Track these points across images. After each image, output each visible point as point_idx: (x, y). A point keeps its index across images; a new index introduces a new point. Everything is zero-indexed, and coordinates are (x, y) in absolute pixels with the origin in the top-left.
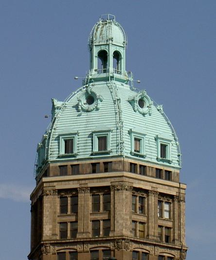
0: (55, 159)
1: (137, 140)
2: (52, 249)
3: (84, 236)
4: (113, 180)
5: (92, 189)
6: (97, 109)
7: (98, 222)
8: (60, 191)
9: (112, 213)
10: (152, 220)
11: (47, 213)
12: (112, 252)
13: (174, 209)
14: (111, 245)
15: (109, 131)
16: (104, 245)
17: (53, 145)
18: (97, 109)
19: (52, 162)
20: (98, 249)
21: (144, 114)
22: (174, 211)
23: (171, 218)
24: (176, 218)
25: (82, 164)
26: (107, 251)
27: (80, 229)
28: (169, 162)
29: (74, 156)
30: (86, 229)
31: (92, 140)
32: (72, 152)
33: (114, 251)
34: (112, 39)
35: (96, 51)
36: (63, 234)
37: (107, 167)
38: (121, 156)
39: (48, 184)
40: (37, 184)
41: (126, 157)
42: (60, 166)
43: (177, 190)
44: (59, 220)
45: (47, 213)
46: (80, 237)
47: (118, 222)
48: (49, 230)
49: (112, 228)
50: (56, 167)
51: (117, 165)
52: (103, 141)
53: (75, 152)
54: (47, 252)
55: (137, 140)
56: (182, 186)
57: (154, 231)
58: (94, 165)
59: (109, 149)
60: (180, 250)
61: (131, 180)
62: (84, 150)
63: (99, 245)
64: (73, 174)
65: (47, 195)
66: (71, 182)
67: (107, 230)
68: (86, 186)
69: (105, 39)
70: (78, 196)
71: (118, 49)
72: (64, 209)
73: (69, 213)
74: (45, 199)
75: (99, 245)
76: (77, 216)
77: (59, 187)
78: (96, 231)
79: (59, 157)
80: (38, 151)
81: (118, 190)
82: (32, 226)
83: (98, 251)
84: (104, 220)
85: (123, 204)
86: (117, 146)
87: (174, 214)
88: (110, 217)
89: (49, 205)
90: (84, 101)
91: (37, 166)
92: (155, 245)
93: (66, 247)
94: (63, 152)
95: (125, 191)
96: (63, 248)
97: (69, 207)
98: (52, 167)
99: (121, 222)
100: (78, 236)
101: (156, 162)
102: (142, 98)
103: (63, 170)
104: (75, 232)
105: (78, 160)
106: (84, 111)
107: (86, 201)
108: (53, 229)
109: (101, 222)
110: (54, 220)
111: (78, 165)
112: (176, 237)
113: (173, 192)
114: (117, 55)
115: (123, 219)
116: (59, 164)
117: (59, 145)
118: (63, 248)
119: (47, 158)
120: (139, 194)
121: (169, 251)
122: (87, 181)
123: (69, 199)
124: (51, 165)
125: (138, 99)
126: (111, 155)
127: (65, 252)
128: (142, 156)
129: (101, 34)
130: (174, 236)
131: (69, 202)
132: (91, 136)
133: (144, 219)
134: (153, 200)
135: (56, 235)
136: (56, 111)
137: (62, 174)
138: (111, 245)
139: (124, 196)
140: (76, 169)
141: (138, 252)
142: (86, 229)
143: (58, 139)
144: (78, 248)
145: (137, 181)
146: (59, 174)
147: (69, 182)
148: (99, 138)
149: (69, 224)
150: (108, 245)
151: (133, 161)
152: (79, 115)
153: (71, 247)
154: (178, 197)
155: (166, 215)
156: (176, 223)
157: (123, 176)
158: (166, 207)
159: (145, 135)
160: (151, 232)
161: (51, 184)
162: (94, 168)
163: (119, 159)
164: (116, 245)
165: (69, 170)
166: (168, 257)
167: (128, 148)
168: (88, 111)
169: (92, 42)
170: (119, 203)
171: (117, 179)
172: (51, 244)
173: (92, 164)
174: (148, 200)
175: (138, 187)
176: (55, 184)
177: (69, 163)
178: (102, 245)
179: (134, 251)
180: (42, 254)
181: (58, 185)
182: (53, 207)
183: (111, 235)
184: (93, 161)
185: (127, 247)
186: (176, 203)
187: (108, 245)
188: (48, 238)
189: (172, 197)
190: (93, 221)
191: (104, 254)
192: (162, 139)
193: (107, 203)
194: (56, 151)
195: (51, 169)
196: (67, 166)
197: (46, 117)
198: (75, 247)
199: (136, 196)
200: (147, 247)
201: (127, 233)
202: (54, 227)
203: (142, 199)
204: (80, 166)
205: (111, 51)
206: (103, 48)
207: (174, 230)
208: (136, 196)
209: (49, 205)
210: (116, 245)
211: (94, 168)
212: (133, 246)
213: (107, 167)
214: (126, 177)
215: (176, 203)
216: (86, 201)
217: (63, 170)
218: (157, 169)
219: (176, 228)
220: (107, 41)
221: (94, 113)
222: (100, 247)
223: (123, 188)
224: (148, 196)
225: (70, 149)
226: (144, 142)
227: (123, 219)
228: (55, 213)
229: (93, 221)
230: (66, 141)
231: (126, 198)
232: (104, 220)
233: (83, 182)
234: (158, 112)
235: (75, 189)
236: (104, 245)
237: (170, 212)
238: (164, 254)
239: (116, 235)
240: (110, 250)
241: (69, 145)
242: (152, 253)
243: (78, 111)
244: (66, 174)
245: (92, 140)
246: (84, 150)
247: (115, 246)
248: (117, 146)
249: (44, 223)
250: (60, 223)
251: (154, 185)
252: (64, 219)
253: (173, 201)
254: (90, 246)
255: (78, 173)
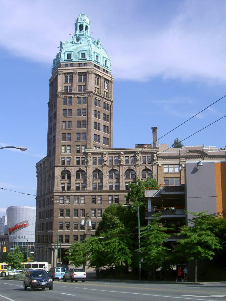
0: (63, 61)
1: (97, 56)
2: (61, 96)
3: (75, 91)
4: (88, 69)
5: (79, 73)
6: (81, 43)
7: (81, 87)
8: (65, 73)
9: (87, 82)
10: (102, 88)
11: (60, 82)
12: (87, 98)
13: (109, 85)
14: (86, 95)
15: (86, 51)
16: (84, 95)
17: (62, 56)
18: (81, 43)
19: (62, 62)
20: (81, 97)
21: (98, 48)
22: (109, 87)
23: (108, 89)
24: (110, 89)
25: (75, 64)
26: (85, 98)
27: (73, 88)
28: (108, 67)
29: (71, 60)
30: (76, 89)
31: (79, 54)
32: (70, 58)
33: (88, 97)
34: (85, 20)
35: (78, 24)
36: (66, 90)
37: (85, 64)
38: (91, 61)
39: (60, 71)
40: (52, 75)
41: (93, 61)
42: (65, 64)
43: (110, 78)
44: (64, 85)
45: (60, 82)
46: (73, 91)
47: (89, 86)
48: (60, 88)
49: (87, 88)
50: (63, 64)
51: (89, 64)
52: (84, 55)
53: (72, 58)
54: (59, 97)
55: (97, 56)
56: (112, 77)
57: (102, 92)
58: (79, 64)
59: (86, 58)
60: (111, 101)
61: (95, 70)
62: (75, 58)
63: (81, 95)
64: (70, 67)
65: (60, 75)
66: (70, 70)
67: (85, 90)
68: (76, 71)
69: (82, 20)
70: (72, 76)
71: (87, 25)
72: (66, 81)
73: (68, 82)
74: (59, 76)
75: (81, 95)
76: (72, 83)
77: (65, 72)
78: (80, 90)
79: (65, 61)
80: (75, 24)
81: (90, 73)
82: (50, 91)
83: (81, 97)
84: (83, 86)
85: (92, 79)
86: (90, 57)
87: (109, 87)
88: (86, 84)
89: (60, 79)
90: (75, 39)
91: (52, 68)
92: (103, 98)
93: (67, 96)
94: (66, 59)
95: (93, 74)
96: (66, 96)
97: (69, 80)
98: (62, 64)
99: (91, 86)
100: (72, 91)
101: (103, 66)
102: (98, 42)
103: (66, 65)
104: (71, 90)
105: (73, 62)
106: (75, 44)
107: (76, 77)
108: (62, 88)
109: (82, 86)
110: (62, 85)
111: (73, 64)
112: (110, 97)
113: (109, 79)
114: (87, 27)
115: (92, 85)
116: (65, 63)
117: (65, 56)
118: (66, 96)
119: (60, 61)
120: (97, 77)
121: (107, 101)
122: (77, 70)
123: (69, 77)
124: (61, 63)
125: (97, 41)
126: (87, 60)
127: (67, 98)
128: (99, 63)
129: (81, 18)
130: (109, 96)
131: (69, 78)
132: (79, 53)
133: (99, 87)
134: (102, 80)
135: (63, 91)
136: (63, 45)
137: (66, 67)
138: (86, 95)
139: (92, 76)
140: (72, 65)
141: (97, 99)
142: (76, 89)
143: (65, 53)
144: (73, 96)
145: (97, 71)
146: (65, 67)
147: (69, 70)
148: (82, 54)
149: (68, 87)
150: (85, 95)
151: (96, 64)
152: (73, 45)
153: (69, 96)
154: (111, 81)
155: (106, 88)
156: (110, 91)
157: (92, 68)
158: (106, 85)
159: (100, 55)
160: (101, 93)
161: (62, 71)
162: (80, 65)
163: (90, 62)
164: (89, 95)
165: (69, 65)
166: (107, 104)
167: (94, 58)
168: (77, 44)
169: (77, 21)
170: (90, 78)
171: (90, 69)
172: (61, 94)
173: (79, 63)
174: (100, 80)
175: (97, 73)
176: (63, 70)
177: (69, 63)
178: (83, 95)
179: (95, 99)
180: (57, 98)
181: (64, 71)
182: (62, 80)
183: (86, 91)
184: (79, 62)
185: (93, 96)
186: (110, 83)
187: (85, 95)
188: (60, 92)
189: (108, 80)
190: (79, 86)
191: (83, 99)
192: (106, 58)
193: (85, 80)
194: (63, 58)
195: (61, 65)
196: (68, 64)
197: (58, 48)
198: (71, 96)
199: (96, 78)
200: (100, 98)
201: (93, 91)
202: (62, 87)
203: (98, 79)
204: (74, 64)
205: (85, 25)
206: (81, 23)
207: (109, 94)
208: (96, 78)
209: (60, 79)
210: (89, 95)
211: (80, 65)
212: (95, 96)
213: (85, 64)
214: (93, 69)
215: (110, 83)
216: (76, 77)
217: (66, 65)
218: (103, 69)
219: (110, 93)
220: (83, 21)
221: (79, 45)
222: (82, 96)
223: (92, 73)
224: (100, 78)
225: (69, 57)
226: (99, 57)
227: (92, 85)
228: (63, 82)
229: (79, 86)
230: (68, 55)
231: (93, 77)
232: (83, 86)
233: (75, 70)
234: (103, 49)
235: (72, 73)
236: (84, 95)
237: (107, 87)
238: (106, 102)
239: (88, 91)
240: (86, 97)
241: (69, 56)
242: (102, 100)
243: (73, 44)
244: (68, 67)
245: (79, 54)
246: (75, 58)
247: (88, 95)
248: (90, 57)
249: (58, 86)
250: (65, 86)
251: (103, 74)
252: (67, 85)
253: (109, 82)
254: (78, 95)
255: (73, 67)
